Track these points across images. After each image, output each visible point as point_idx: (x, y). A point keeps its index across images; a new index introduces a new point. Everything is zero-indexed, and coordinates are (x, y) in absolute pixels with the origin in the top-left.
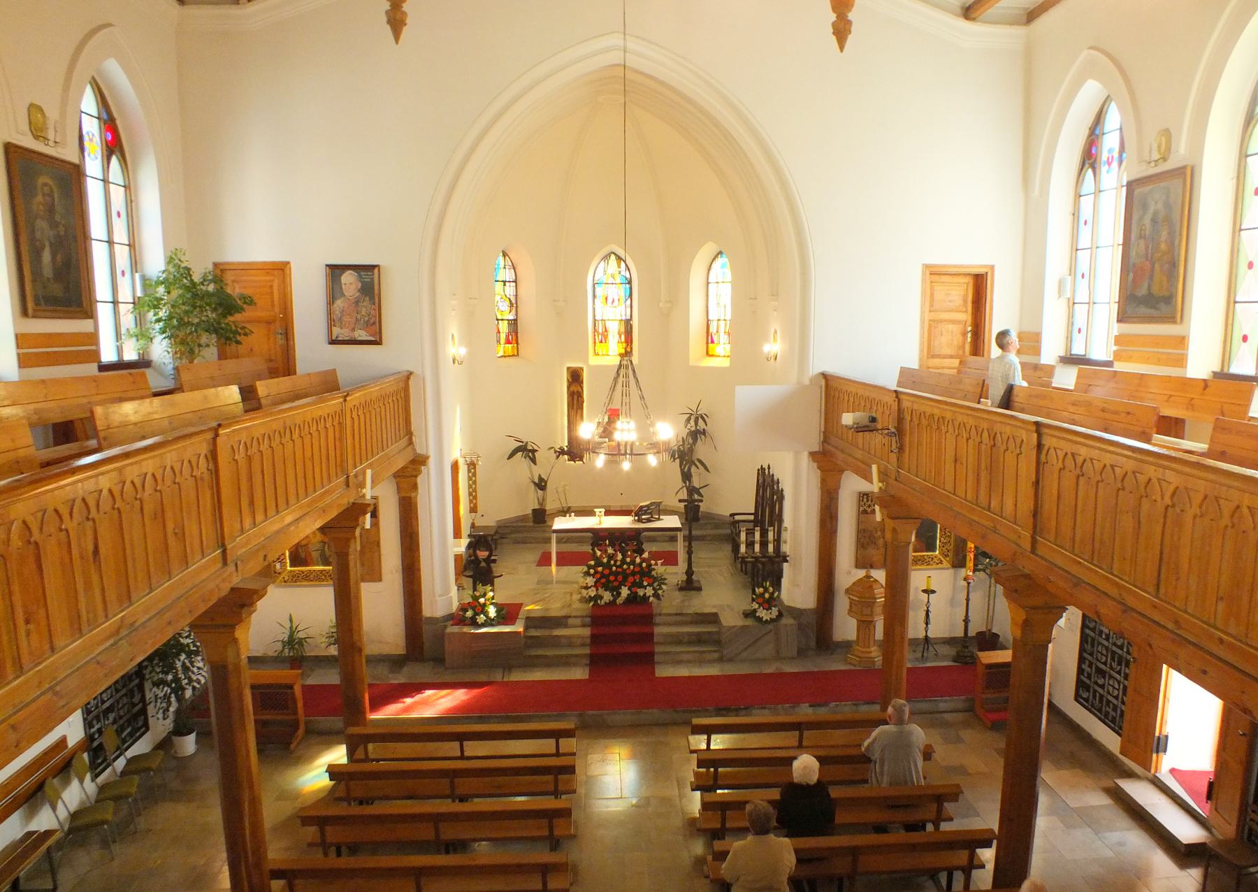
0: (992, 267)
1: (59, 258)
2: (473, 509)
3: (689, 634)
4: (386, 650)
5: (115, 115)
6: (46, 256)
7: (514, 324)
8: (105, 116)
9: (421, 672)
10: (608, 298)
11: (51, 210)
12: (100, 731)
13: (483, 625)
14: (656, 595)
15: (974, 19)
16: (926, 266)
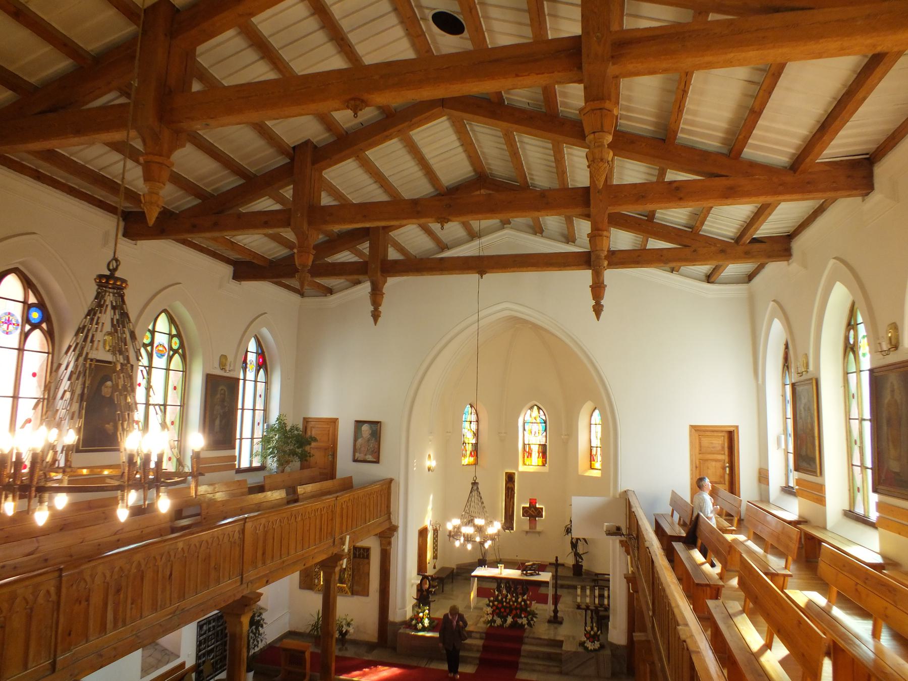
0: (737, 427)
2: (435, 557)
3: (544, 653)
4: (366, 638)
7: (476, 447)
10: (532, 430)
12: (204, 662)
14: (529, 624)
15: (712, 283)
16: (692, 427)
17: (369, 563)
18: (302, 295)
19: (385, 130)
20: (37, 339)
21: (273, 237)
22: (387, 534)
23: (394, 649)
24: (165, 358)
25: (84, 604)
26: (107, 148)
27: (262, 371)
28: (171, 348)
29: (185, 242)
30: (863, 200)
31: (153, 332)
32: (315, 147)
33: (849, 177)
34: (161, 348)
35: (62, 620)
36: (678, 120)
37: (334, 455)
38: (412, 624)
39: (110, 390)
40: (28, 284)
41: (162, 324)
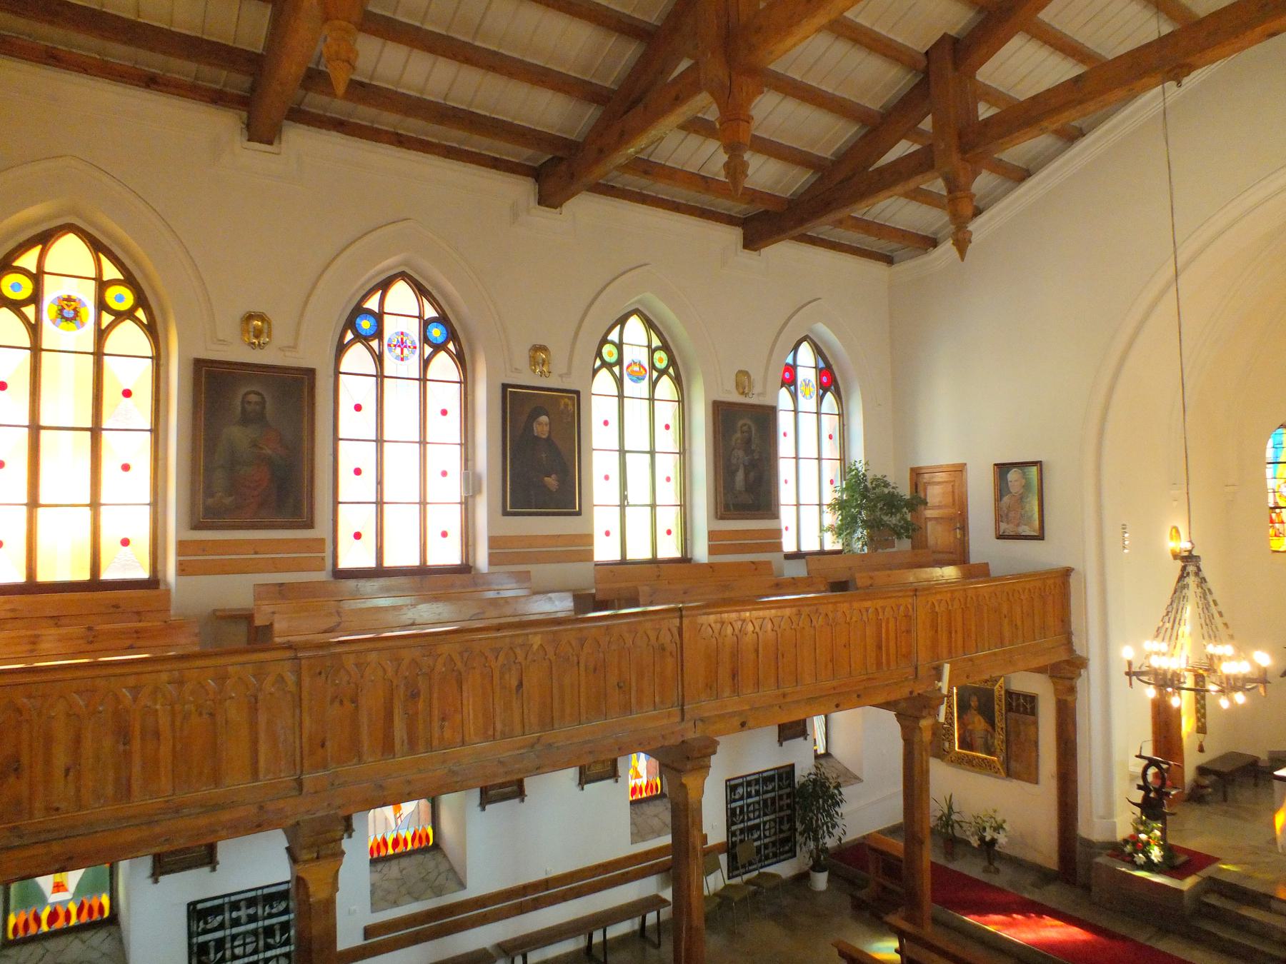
1: (752, 475)
2: (1201, 729)
4: (1039, 859)
5: (832, 361)
6: (740, 476)
8: (822, 365)
9: (1051, 895)
11: (748, 442)
13: (1141, 868)
17: (1036, 723)
18: (889, 260)
20: (443, 365)
22: (1066, 671)
23: (1087, 888)
24: (645, 384)
25: (349, 706)
27: (829, 397)
28: (653, 366)
31: (620, 346)
34: (636, 368)
35: (307, 721)
37: (964, 529)
38: (1125, 851)
39: (546, 429)
40: (421, 291)
41: (635, 328)
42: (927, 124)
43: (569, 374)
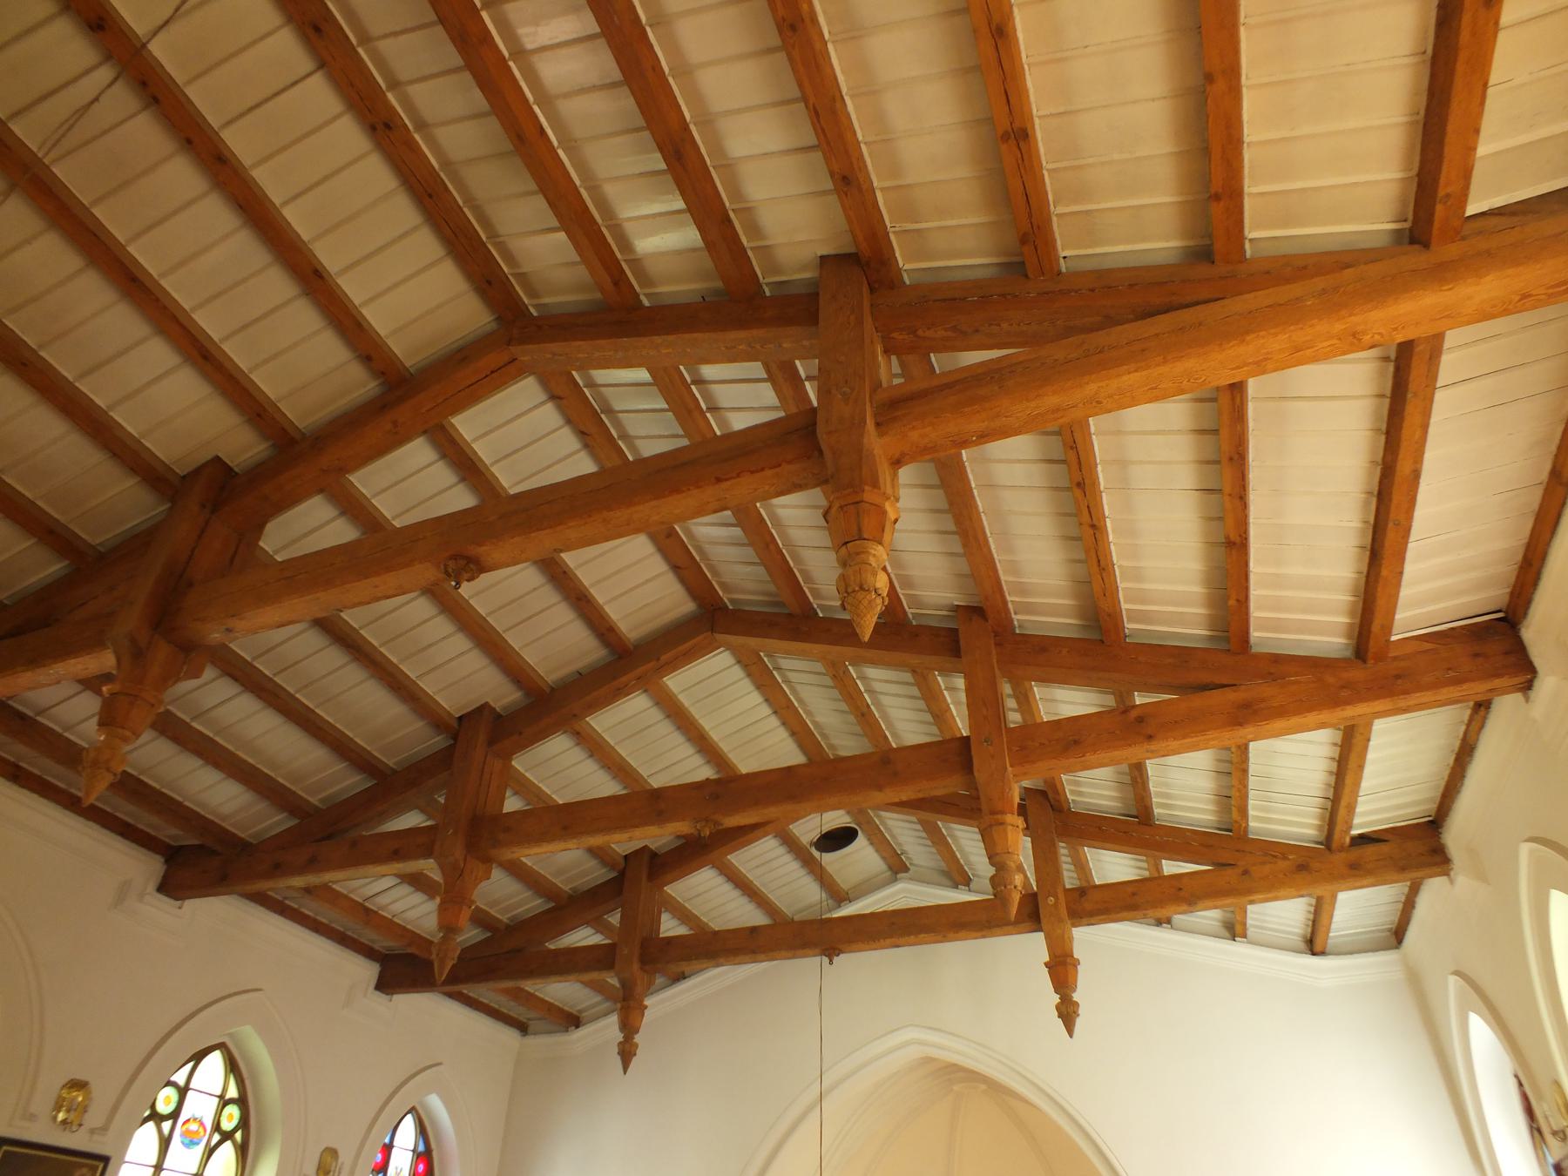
5: (433, 1146)
8: (421, 1148)
15: (1323, 953)
18: (523, 1028)
19: (614, 678)
21: (590, 985)
24: (199, 1150)
26: (80, 687)
28: (217, 1127)
29: (262, 900)
30: (1527, 700)
31: (183, 1091)
32: (499, 716)
33: (1476, 655)
34: (193, 1126)
36: (1110, 590)
41: (213, 1069)
42: (615, 919)
43: (104, 1129)
